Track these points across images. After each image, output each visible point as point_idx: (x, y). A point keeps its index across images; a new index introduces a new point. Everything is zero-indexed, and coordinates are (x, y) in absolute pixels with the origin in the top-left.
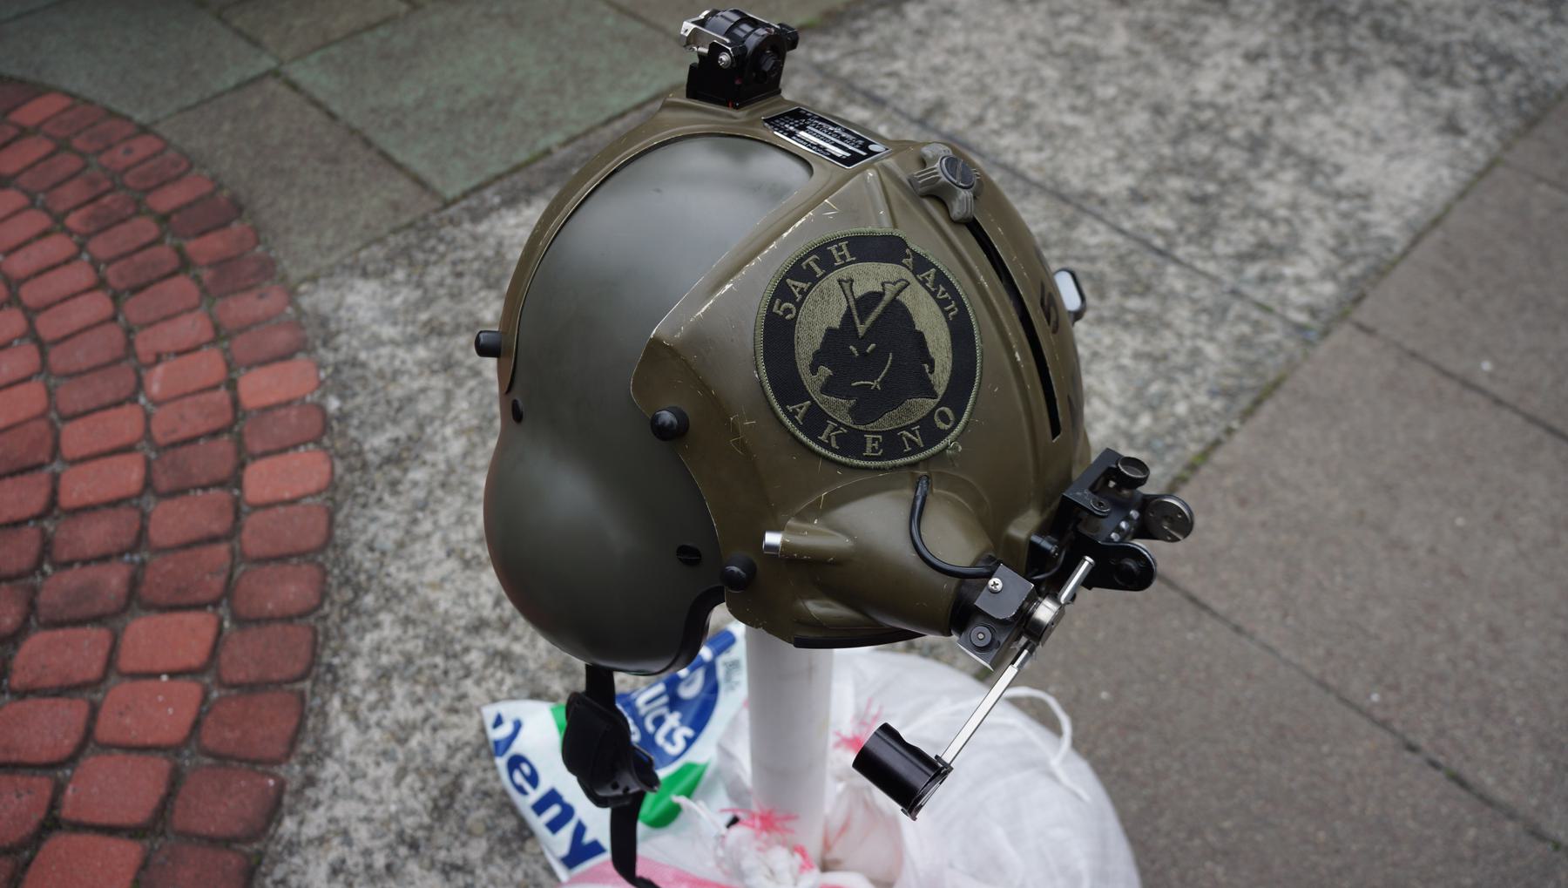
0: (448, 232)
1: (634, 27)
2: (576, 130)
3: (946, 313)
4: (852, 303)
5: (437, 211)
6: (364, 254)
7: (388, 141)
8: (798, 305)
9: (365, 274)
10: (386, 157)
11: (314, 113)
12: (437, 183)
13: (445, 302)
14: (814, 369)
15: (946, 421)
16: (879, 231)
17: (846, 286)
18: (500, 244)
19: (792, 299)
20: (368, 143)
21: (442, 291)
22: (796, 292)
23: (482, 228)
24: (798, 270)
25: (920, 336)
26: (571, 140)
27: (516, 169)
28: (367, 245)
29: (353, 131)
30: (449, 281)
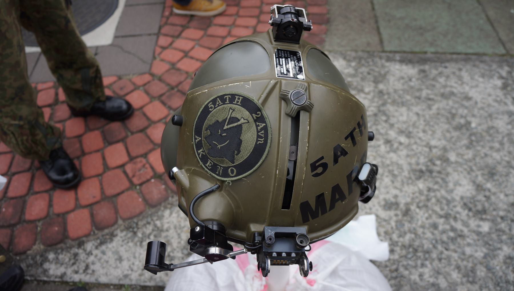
0: (377, 60)
1: (488, 27)
2: (440, 50)
3: (257, 141)
4: (229, 117)
5: (379, 52)
6: (349, 53)
7: (382, 24)
8: (215, 108)
9: (345, 58)
10: (378, 29)
11: (369, 6)
12: (386, 43)
13: (359, 79)
14: (206, 130)
15: (232, 173)
16: (256, 101)
17: (231, 111)
18: (388, 72)
19: (215, 105)
20: (377, 22)
21: (360, 75)
22: (218, 103)
23: (387, 64)
24: (222, 98)
25: (241, 141)
26: (436, 53)
27: (412, 53)
28: (352, 50)
29: (375, 17)
30: (365, 74)
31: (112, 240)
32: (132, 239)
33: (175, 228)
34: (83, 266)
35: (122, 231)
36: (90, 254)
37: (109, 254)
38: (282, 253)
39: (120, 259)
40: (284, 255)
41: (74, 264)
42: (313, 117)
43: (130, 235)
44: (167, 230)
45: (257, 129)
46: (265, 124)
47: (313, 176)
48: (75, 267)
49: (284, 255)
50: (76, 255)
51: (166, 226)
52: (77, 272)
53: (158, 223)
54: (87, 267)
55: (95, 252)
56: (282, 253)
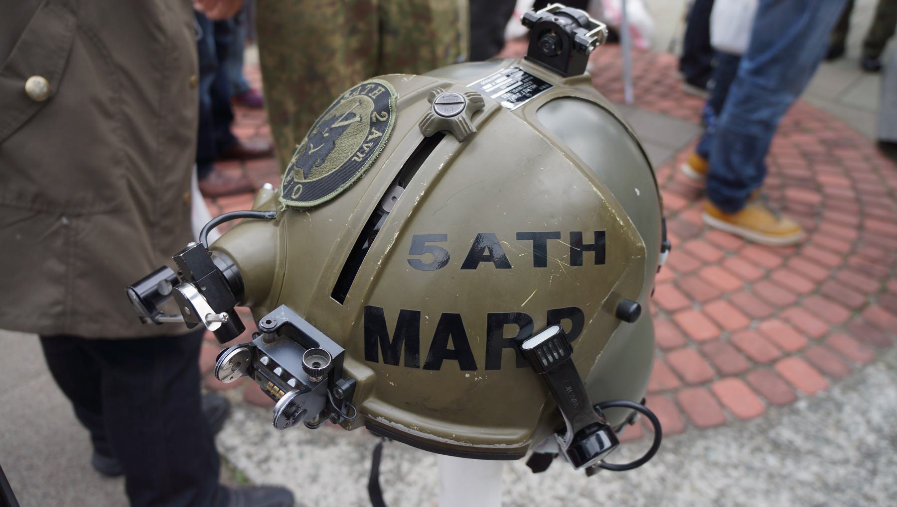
3: (356, 155)
31: (325, 446)
32: (353, 463)
33: (424, 488)
34: (263, 453)
35: (349, 443)
36: (284, 444)
37: (308, 461)
38: (279, 366)
39: (314, 479)
40: (278, 371)
41: (255, 444)
42: (463, 161)
43: (355, 456)
44: (409, 484)
45: (367, 137)
46: (380, 134)
47: (409, 261)
48: (252, 450)
49: (278, 371)
50: (267, 435)
51: (412, 477)
52: (249, 456)
53: (405, 466)
54: (266, 460)
55: (294, 448)
56: (279, 366)
